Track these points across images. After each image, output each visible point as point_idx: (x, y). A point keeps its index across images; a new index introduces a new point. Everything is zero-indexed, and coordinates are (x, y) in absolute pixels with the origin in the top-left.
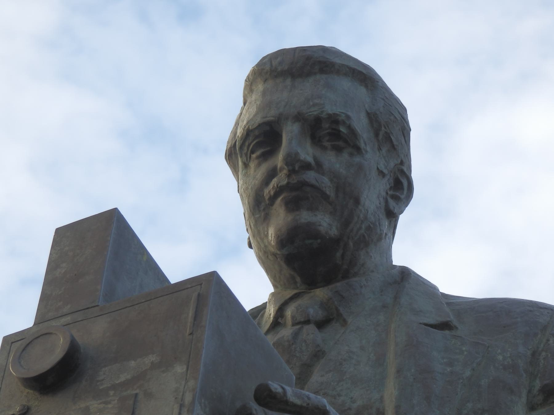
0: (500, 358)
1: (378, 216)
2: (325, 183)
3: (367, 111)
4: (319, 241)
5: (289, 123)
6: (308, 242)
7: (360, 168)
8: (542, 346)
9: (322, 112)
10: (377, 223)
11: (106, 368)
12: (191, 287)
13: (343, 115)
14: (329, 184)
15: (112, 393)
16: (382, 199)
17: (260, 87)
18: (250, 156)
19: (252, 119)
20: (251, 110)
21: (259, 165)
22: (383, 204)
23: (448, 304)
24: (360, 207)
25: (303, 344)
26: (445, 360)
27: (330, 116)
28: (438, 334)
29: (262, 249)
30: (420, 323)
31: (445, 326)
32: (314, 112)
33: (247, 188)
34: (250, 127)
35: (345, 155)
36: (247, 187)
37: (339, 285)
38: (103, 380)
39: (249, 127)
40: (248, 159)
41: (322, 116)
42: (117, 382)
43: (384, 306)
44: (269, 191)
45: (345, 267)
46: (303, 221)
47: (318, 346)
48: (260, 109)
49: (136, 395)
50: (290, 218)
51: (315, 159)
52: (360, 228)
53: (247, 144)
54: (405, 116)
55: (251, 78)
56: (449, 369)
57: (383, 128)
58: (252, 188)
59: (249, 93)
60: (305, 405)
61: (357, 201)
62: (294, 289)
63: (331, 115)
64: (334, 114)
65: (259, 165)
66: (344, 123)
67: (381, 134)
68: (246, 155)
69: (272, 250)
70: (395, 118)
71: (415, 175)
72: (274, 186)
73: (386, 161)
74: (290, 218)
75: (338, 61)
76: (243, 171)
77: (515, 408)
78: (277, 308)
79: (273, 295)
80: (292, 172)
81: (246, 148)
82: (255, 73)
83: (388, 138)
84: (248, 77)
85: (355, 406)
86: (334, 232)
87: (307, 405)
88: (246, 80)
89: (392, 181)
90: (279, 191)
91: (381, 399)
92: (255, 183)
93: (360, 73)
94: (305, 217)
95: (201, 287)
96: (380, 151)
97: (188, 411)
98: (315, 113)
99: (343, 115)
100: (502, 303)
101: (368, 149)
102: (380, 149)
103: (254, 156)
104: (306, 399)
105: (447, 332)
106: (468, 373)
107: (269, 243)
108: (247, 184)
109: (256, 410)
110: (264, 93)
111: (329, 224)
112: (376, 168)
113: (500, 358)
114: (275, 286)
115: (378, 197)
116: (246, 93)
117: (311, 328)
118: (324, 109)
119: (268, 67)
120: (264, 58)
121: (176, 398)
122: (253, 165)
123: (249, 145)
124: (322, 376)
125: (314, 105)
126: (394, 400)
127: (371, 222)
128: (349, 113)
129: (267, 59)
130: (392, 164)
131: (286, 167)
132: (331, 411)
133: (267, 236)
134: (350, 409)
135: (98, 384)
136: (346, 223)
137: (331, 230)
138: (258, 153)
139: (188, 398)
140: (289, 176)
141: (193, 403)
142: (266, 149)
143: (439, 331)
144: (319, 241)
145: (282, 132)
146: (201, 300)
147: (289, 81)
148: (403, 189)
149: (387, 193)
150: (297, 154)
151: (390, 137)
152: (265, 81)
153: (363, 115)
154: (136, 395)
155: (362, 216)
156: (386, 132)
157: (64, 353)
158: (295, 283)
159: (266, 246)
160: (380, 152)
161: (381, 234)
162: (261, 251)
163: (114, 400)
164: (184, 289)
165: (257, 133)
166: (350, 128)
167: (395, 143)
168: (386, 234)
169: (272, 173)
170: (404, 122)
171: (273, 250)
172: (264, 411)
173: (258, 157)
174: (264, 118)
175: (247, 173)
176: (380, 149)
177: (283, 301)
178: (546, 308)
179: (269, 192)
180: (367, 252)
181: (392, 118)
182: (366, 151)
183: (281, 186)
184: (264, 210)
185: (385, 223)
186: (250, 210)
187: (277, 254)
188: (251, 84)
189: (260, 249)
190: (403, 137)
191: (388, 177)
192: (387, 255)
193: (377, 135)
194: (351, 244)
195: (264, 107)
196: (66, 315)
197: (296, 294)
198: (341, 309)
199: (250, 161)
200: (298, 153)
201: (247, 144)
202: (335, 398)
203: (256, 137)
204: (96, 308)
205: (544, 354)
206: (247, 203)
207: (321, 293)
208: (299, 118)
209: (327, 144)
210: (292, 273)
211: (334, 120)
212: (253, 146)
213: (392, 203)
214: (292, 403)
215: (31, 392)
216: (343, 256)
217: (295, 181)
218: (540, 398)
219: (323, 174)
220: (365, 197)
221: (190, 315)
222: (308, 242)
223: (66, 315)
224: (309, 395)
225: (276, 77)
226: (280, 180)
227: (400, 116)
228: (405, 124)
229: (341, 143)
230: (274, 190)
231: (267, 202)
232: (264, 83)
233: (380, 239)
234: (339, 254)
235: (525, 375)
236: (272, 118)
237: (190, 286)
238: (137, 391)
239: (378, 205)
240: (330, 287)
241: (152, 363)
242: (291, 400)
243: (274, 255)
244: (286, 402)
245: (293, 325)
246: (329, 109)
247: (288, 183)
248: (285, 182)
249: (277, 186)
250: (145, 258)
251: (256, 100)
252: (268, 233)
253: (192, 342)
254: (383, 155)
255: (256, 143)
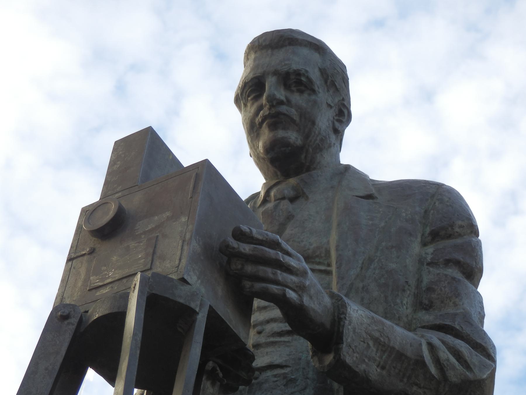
0: (404, 214)
1: (328, 132)
2: (293, 113)
3: (319, 68)
4: (290, 148)
5: (270, 77)
6: (283, 149)
7: (315, 102)
8: (431, 206)
9: (290, 69)
10: (327, 137)
11: (141, 222)
12: (192, 170)
13: (304, 70)
14: (295, 113)
15: (143, 236)
16: (330, 122)
17: (253, 56)
18: (247, 99)
19: (247, 76)
20: (247, 70)
21: (253, 104)
22: (331, 125)
23: (373, 185)
24: (316, 127)
25: (280, 212)
26: (368, 217)
27: (295, 71)
28: (365, 201)
29: (256, 156)
30: (354, 196)
31: (369, 197)
32: (285, 69)
33: (246, 119)
34: (246, 81)
35: (306, 95)
36: (246, 118)
37: (303, 176)
38: (138, 229)
39: (245, 80)
40: (246, 101)
41: (290, 71)
42: (146, 230)
43: (332, 187)
44: (258, 119)
45: (308, 164)
46: (279, 136)
47: (290, 212)
48: (253, 69)
49: (157, 236)
50: (271, 135)
51: (287, 98)
52: (316, 140)
53: (245, 91)
54: (344, 71)
55: (247, 51)
56: (370, 222)
57: (330, 78)
58: (248, 118)
59: (246, 61)
60: (264, 239)
61: (314, 123)
62: (277, 179)
63: (295, 70)
64: (298, 70)
65: (253, 104)
66: (304, 75)
67: (329, 81)
68: (245, 98)
69: (262, 155)
70: (338, 71)
71: (353, 109)
72: (261, 116)
73: (332, 98)
74: (271, 135)
75: (300, 37)
76: (244, 109)
77: (413, 245)
78: (265, 191)
79: (264, 184)
80: (272, 106)
81: (244, 94)
82: (249, 48)
83: (333, 84)
84: (246, 51)
85: (312, 247)
86: (299, 142)
87: (266, 239)
88: (245, 54)
89: (337, 110)
90: (264, 119)
91: (328, 242)
92: (250, 115)
93: (315, 44)
94: (281, 133)
95: (198, 169)
96: (329, 92)
97: (187, 244)
98: (286, 70)
99: (304, 70)
100: (406, 182)
101: (320, 91)
102: (328, 91)
103: (249, 98)
104: (265, 236)
105: (371, 201)
106: (383, 224)
107: (260, 152)
108: (246, 117)
109: (232, 242)
110: (255, 60)
111: (296, 138)
112: (326, 102)
113: (404, 214)
114: (266, 179)
115: (328, 121)
116: (245, 61)
117: (286, 202)
118: (291, 67)
119: (257, 44)
120: (255, 38)
121: (181, 237)
122: (249, 105)
123: (246, 92)
124: (292, 230)
125: (285, 65)
126: (335, 242)
127: (323, 136)
128: (307, 69)
129: (256, 39)
130: (336, 100)
131: (268, 103)
132: (282, 243)
133: (258, 147)
134: (309, 249)
135: (136, 231)
136: (307, 137)
137: (297, 141)
138: (252, 97)
139: (188, 236)
140: (270, 109)
141: (191, 238)
142: (256, 94)
143: (365, 200)
144: (290, 148)
145: (265, 83)
146: (198, 177)
147: (269, 52)
148: (344, 115)
149: (334, 118)
150: (274, 95)
151: (334, 83)
152: (256, 52)
153: (317, 70)
154: (157, 236)
155: (317, 132)
156: (332, 81)
157: (115, 214)
158: (277, 176)
159: (258, 154)
160: (328, 93)
161: (330, 144)
162: (255, 157)
163: (144, 241)
164: (188, 171)
165: (250, 84)
166: (308, 78)
167: (338, 87)
168: (334, 144)
169: (260, 108)
170: (344, 74)
171: (262, 156)
172: (237, 243)
173: (252, 99)
174: (254, 74)
175: (246, 110)
176: (328, 91)
177: (269, 186)
178: (434, 184)
179: (259, 120)
180: (322, 155)
181: (336, 71)
182: (319, 92)
183: (265, 116)
184: (256, 131)
185: (333, 137)
186: (248, 132)
187: (265, 158)
188: (248, 55)
189: (255, 156)
190: (343, 83)
191: (334, 108)
192: (335, 157)
193: (326, 82)
194: (311, 150)
195: (255, 68)
196: (118, 192)
197: (277, 182)
198: (305, 190)
199: (247, 102)
200: (275, 94)
201: (245, 91)
202: (300, 243)
203: (250, 87)
204: (136, 187)
205: (432, 211)
206: (246, 127)
207: (293, 181)
208: (276, 73)
209: (294, 89)
210: (275, 170)
211: (298, 73)
212: (249, 92)
213: (337, 124)
214: (256, 238)
215: (96, 239)
216: (306, 157)
217: (274, 112)
218: (430, 238)
219: (292, 107)
220: (319, 120)
221: (191, 186)
222: (283, 149)
223: (118, 192)
224: (267, 233)
225: (262, 49)
226: (265, 111)
227: (341, 70)
228: (345, 75)
229: (303, 88)
230: (261, 118)
231: (258, 126)
232: (255, 54)
233: (330, 146)
234: (303, 156)
235: (419, 225)
236: (259, 74)
237: (192, 169)
238: (158, 234)
239: (328, 125)
240: (298, 177)
241: (168, 217)
242: (255, 236)
243: (263, 159)
244: (252, 238)
245: (275, 200)
246: (294, 67)
247: (269, 113)
248: (267, 113)
249: (263, 115)
250: (171, 157)
251: (250, 64)
252: (259, 145)
253: (192, 202)
254: (330, 95)
255: (250, 91)
